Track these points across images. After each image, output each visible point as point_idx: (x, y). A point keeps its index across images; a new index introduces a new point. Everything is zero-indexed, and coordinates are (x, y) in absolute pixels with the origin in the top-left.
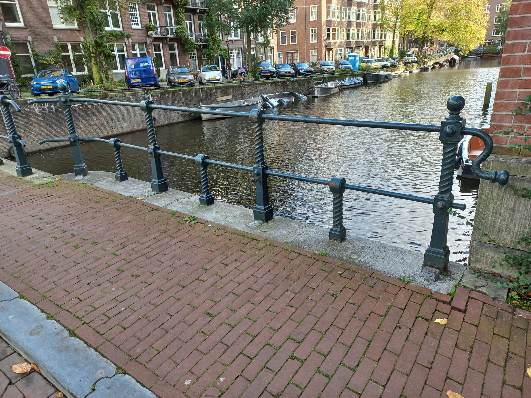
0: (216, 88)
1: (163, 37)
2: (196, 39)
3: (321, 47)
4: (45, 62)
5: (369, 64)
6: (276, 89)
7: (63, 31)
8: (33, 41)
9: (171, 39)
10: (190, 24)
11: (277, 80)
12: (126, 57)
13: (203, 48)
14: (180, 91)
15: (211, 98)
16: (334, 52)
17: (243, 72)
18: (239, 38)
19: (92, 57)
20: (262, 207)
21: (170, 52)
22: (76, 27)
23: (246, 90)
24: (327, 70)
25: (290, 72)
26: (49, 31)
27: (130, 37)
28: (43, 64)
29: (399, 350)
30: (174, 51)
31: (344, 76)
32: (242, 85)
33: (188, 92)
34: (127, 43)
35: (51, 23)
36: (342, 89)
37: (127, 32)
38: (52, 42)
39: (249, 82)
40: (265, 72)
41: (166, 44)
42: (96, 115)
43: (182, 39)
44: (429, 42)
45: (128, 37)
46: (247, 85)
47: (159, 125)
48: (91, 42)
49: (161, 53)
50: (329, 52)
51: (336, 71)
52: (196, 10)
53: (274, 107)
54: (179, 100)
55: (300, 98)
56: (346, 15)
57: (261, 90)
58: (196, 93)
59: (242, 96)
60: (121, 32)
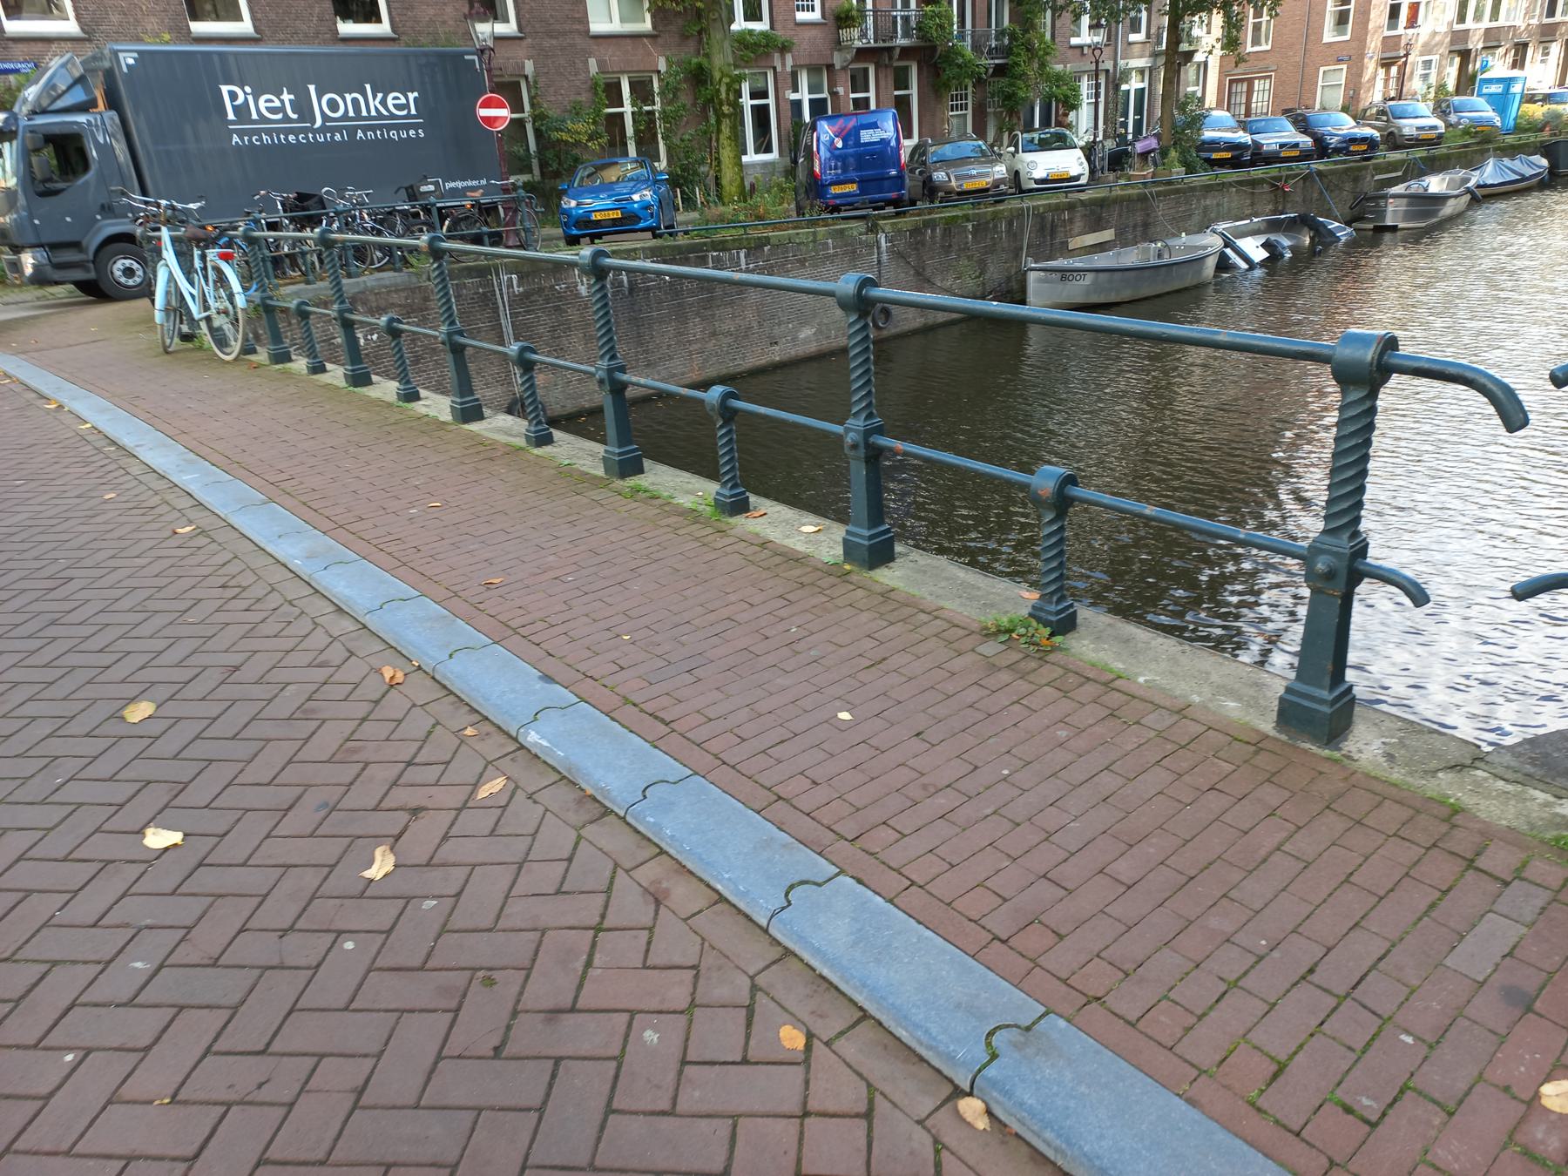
0: (1071, 207)
1: (881, 44)
2: (976, 47)
3: (1362, 56)
4: (565, 136)
5: (1554, 107)
6: (1252, 204)
7: (614, 41)
8: (537, 74)
9: (906, 52)
11: (1257, 172)
13: (993, 75)
14: (967, 218)
17: (1153, 150)
19: (724, 115)
20: (866, 533)
21: (896, 93)
22: (647, 25)
23: (1161, 210)
24: (1415, 133)
25: (1296, 145)
26: (579, 41)
27: (790, 51)
28: (560, 141)
30: (906, 88)
31: (1475, 152)
33: (988, 223)
34: (779, 69)
35: (584, 20)
36: (1483, 197)
37: (781, 34)
38: (582, 76)
39: (1169, 183)
40: (1213, 145)
41: (886, 66)
42: (732, 303)
43: (934, 48)
45: (784, 49)
48: (726, 69)
49: (621, 115)
50: (1388, 73)
51: (1448, 135)
53: (1252, 265)
54: (960, 250)
55: (1331, 233)
57: (1206, 208)
58: (1010, 224)
59: (1146, 232)
60: (763, 34)
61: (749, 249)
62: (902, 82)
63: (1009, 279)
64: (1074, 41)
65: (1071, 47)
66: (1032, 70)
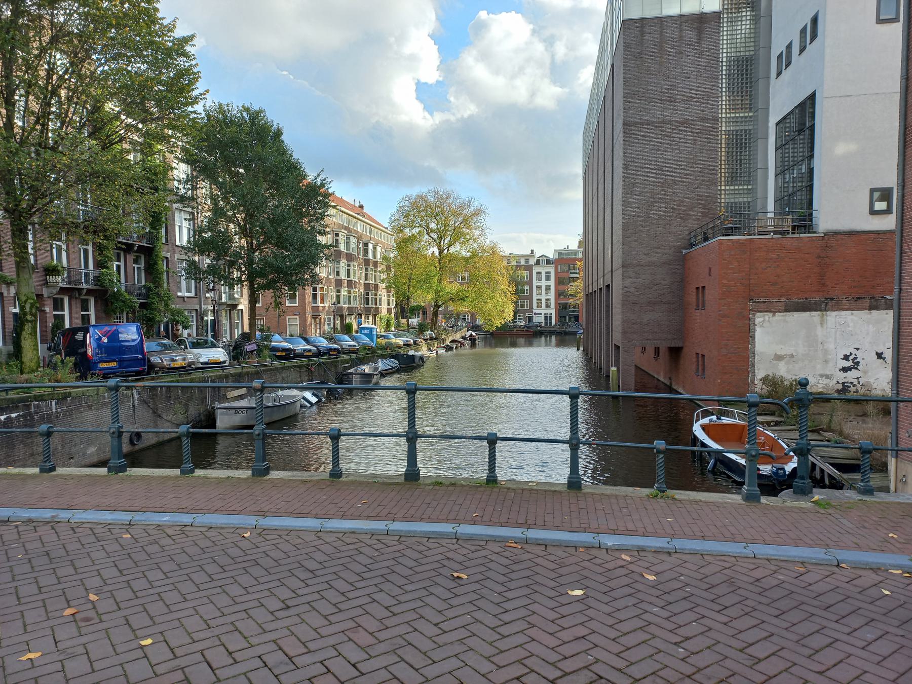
3: (305, 313)
10: (118, 267)
12: (93, 322)
15: (219, 393)
16: (322, 320)
18: (193, 294)
19: (27, 321)
21: (82, 313)
30: (87, 310)
39: (266, 366)
41: (76, 298)
43: (106, 291)
44: (421, 312)
47: (148, 444)
48: (30, 295)
50: (315, 321)
52: (132, 246)
54: (175, 399)
56: (334, 270)
61: (58, 400)
62: (85, 307)
63: (200, 414)
64: (179, 294)
65: (178, 297)
66: (162, 307)
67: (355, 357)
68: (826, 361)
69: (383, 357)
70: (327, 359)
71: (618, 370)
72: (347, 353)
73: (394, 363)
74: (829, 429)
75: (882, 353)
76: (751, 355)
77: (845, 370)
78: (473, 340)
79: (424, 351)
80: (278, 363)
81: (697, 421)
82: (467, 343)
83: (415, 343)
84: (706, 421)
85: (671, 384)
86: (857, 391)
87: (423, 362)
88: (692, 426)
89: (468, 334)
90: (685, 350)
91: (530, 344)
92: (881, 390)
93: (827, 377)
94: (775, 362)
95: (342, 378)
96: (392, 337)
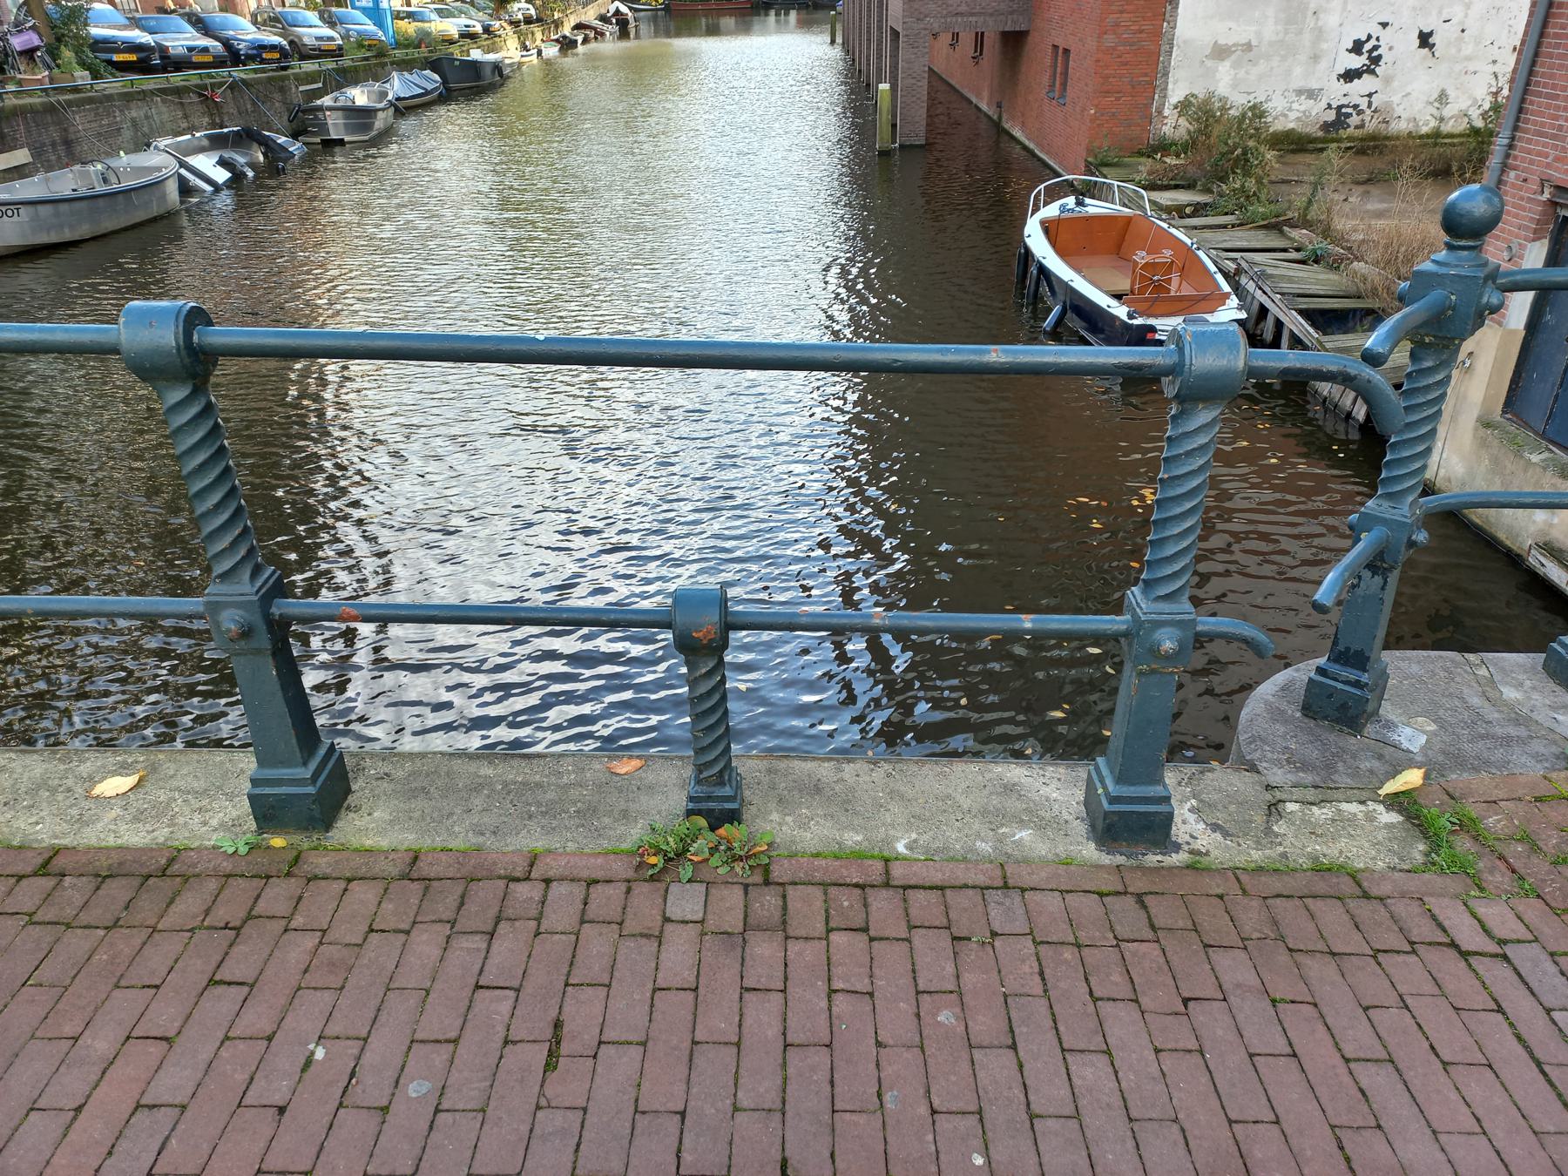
11: (176, 79)
29: (692, 979)
32: (59, 102)
46: (80, 103)
53: (217, 188)
55: (283, 148)
59: (68, 152)
67: (334, 65)
68: (1316, 58)
69: (406, 65)
70: (255, 71)
71: (894, 88)
72: (310, 57)
73: (430, 80)
74: (1305, 223)
75: (1431, 34)
76: (1165, 48)
77: (1349, 76)
78: (623, 23)
79: (510, 51)
80: (113, 84)
81: (1036, 209)
82: (611, 29)
83: (487, 30)
84: (1051, 211)
85: (1000, 117)
86: (1362, 126)
87: (501, 75)
88: (1024, 223)
89: (612, 9)
90: (1032, 40)
91: (745, 29)
92: (1409, 121)
93: (1312, 94)
94: (1209, 63)
95: (303, 122)
96: (434, 16)
